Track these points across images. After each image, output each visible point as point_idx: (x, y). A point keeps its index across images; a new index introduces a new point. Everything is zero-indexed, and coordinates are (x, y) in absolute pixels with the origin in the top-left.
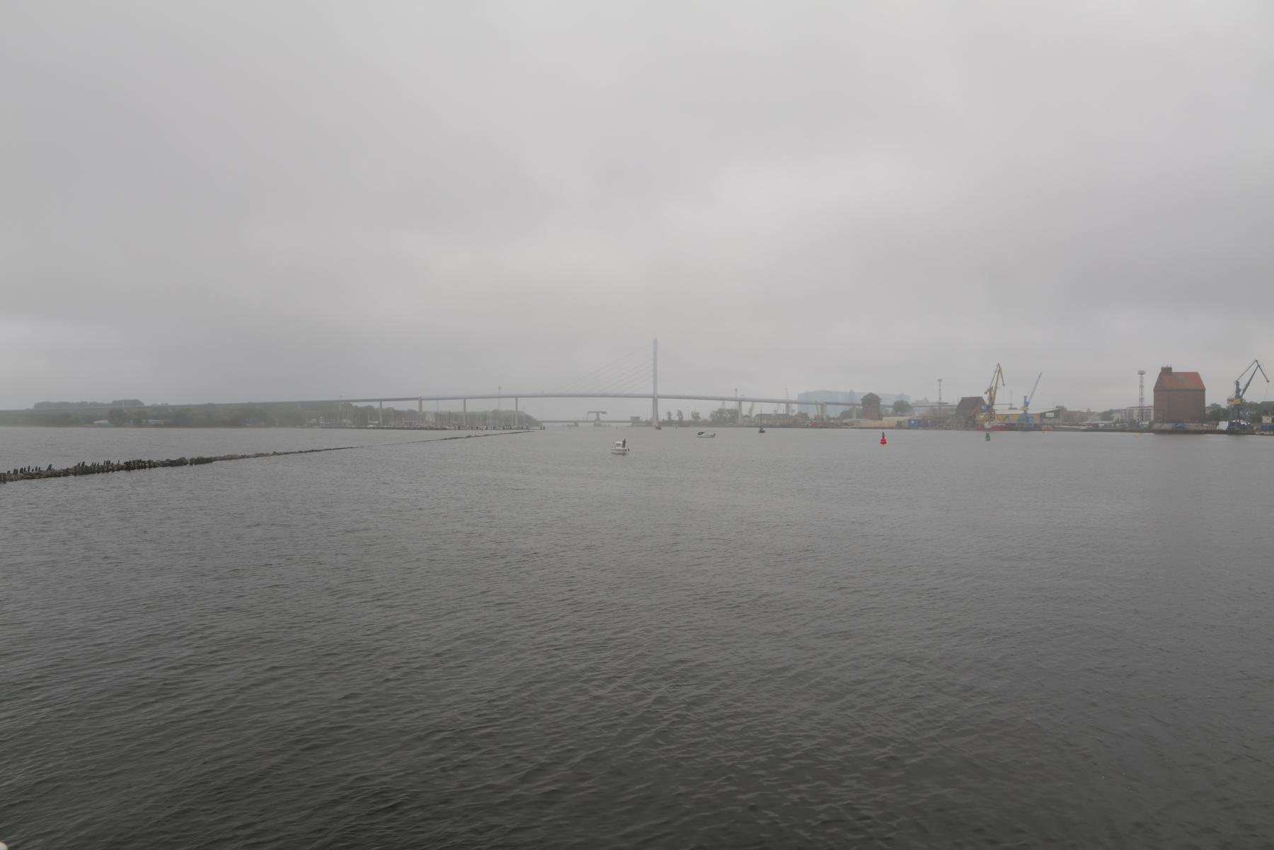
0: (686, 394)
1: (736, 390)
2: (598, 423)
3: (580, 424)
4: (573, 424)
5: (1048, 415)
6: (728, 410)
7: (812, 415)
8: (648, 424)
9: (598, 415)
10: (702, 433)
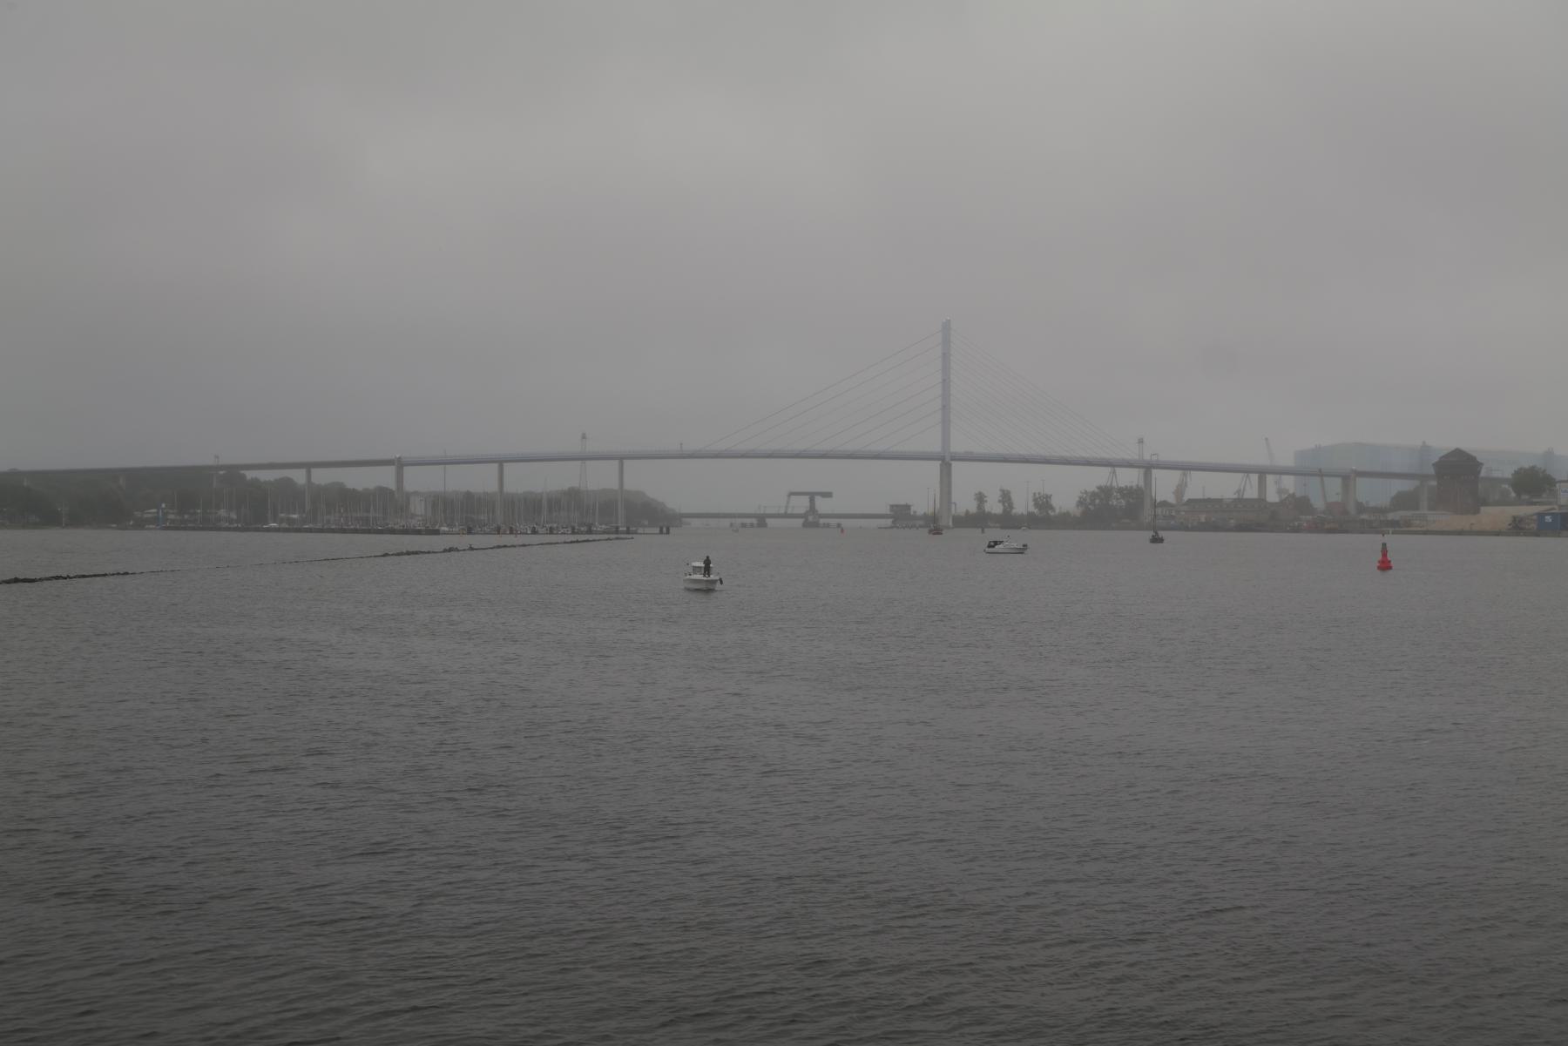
1: (1141, 441)
2: (812, 519)
3: (769, 521)
4: (754, 521)
6: (1120, 490)
7: (1318, 503)
8: (934, 525)
9: (812, 501)
10: (996, 543)
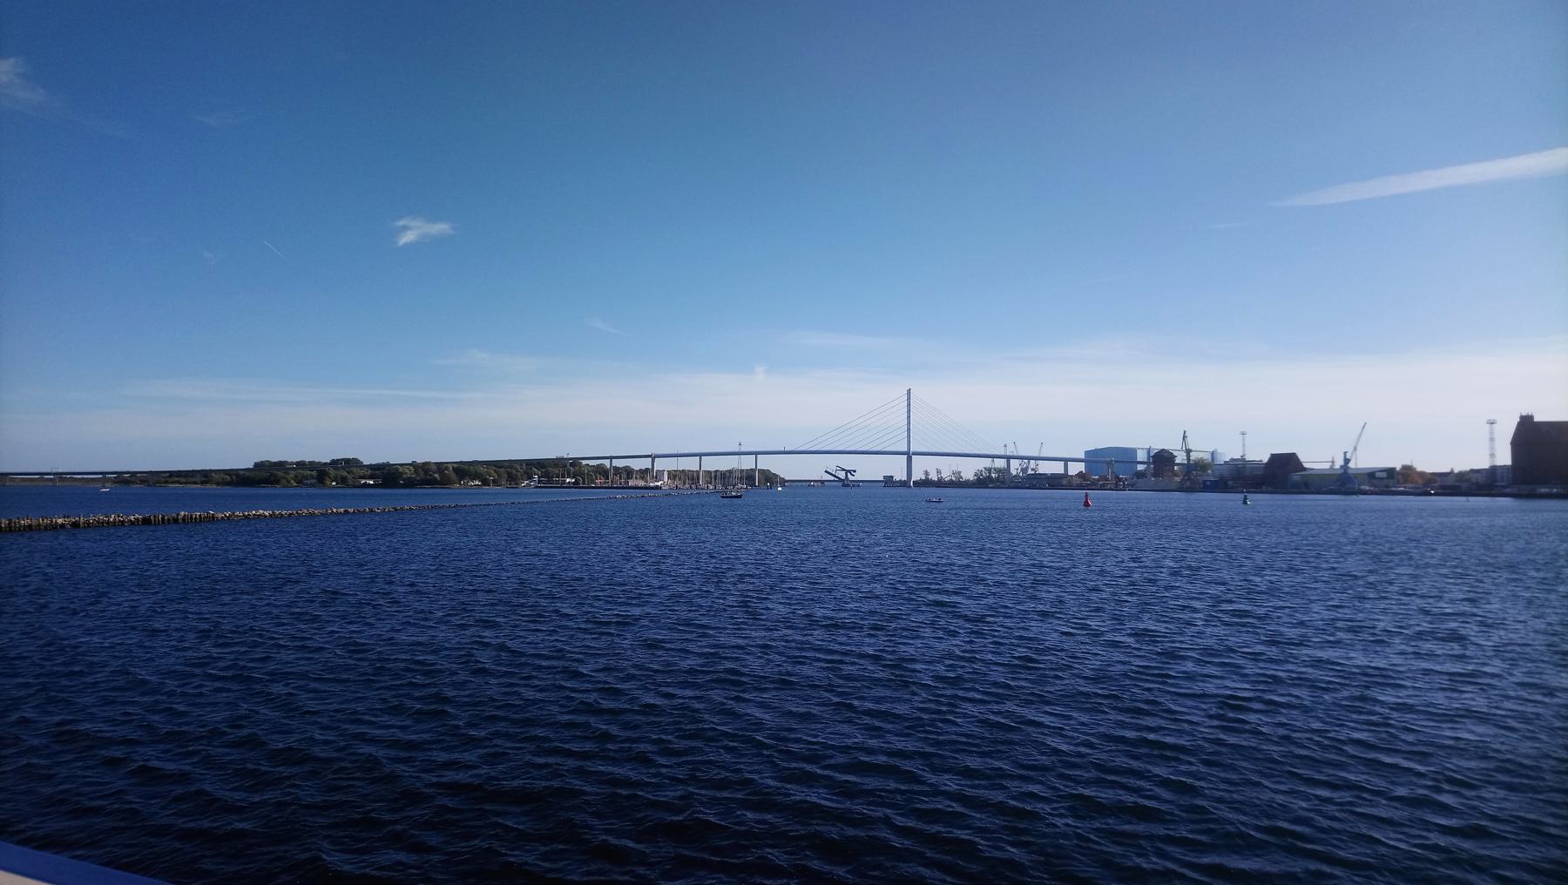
0: (957, 452)
1: (1005, 446)
5: (1378, 475)
